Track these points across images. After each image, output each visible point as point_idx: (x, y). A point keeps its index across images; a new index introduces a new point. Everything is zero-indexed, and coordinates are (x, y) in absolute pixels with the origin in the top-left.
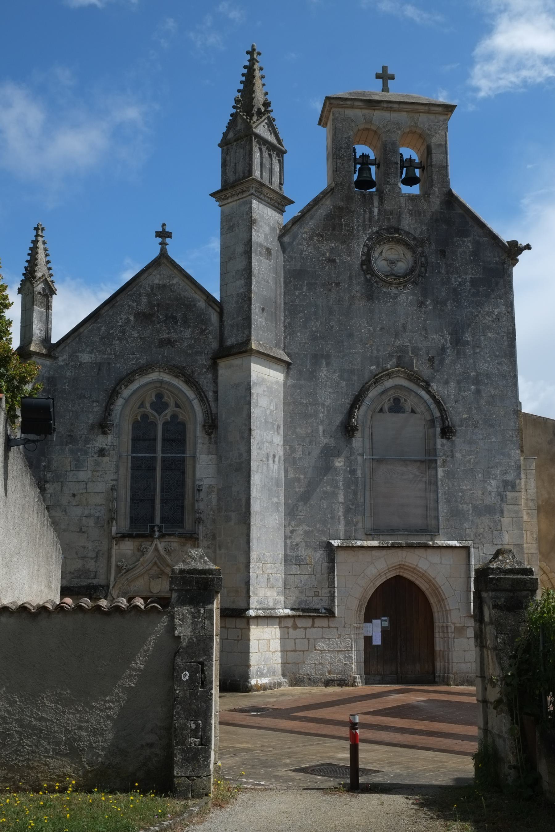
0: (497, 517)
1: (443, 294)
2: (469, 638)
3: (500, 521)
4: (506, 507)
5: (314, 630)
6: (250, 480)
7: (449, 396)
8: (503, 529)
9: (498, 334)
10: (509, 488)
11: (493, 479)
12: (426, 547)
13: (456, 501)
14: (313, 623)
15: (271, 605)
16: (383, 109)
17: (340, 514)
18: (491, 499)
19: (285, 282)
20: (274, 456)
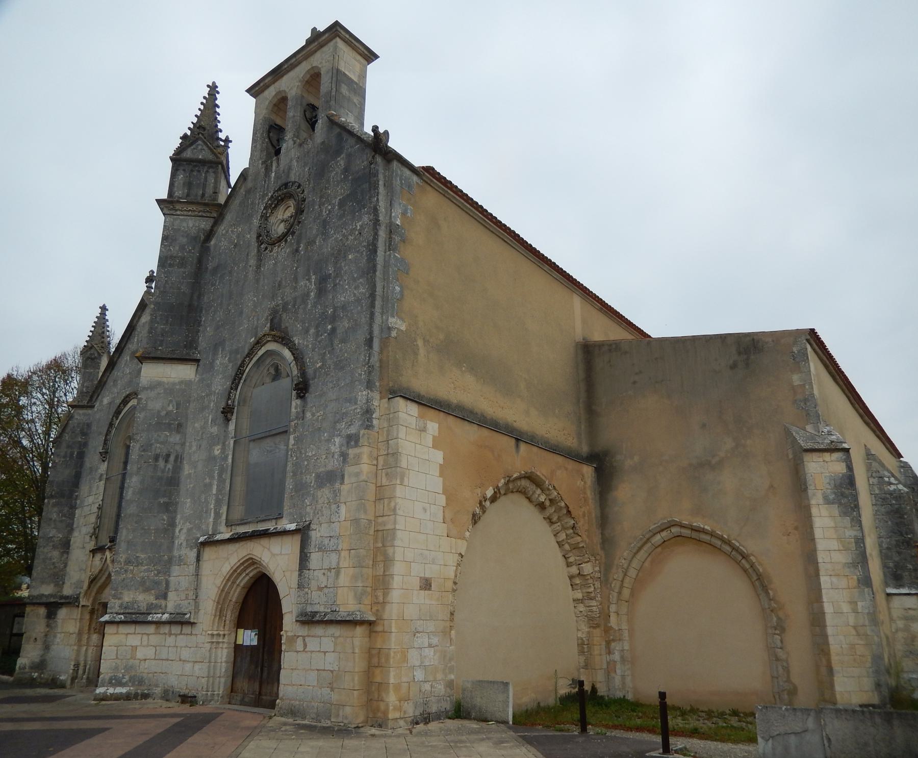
0: (337, 485)
1: (314, 232)
2: (297, 652)
3: (339, 490)
4: (349, 470)
5: (181, 636)
6: (812, 528)
7: (307, 346)
8: (342, 500)
9: (358, 252)
10: (353, 443)
11: (337, 436)
12: (265, 534)
13: (302, 473)
14: (170, 630)
15: (143, 609)
16: (287, 71)
17: (212, 506)
18: (333, 464)
19: (811, 384)
20: (168, 456)
